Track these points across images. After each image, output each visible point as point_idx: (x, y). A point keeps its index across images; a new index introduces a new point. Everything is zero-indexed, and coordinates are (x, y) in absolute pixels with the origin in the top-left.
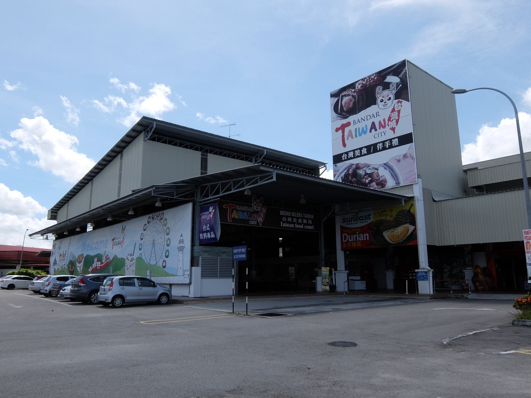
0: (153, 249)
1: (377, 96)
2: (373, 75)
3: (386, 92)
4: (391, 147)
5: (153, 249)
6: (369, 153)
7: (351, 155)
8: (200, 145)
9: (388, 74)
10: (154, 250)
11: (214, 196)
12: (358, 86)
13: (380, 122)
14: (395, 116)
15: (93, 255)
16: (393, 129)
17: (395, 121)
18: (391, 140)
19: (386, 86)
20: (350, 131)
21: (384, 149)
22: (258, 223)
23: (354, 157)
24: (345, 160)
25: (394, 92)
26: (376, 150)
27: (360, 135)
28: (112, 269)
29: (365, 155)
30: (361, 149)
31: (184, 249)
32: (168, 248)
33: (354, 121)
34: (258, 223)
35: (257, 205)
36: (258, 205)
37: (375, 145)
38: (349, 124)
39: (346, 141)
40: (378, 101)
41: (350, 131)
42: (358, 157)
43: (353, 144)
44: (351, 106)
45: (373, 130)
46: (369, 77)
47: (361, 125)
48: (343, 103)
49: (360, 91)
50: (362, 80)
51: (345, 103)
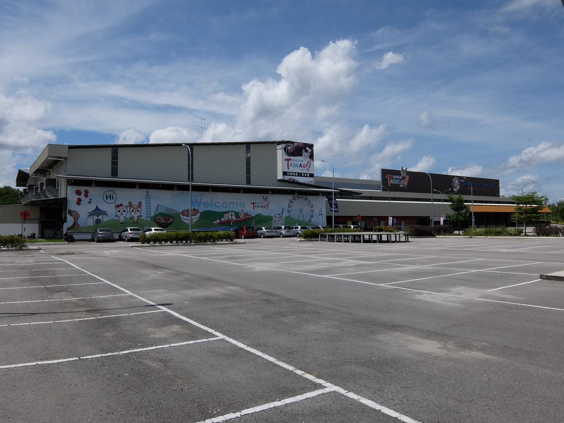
0: (301, 214)
1: (303, 153)
2: (302, 143)
3: (306, 153)
4: (307, 176)
5: (301, 214)
6: (298, 176)
7: (294, 174)
8: (130, 228)
9: (307, 146)
10: (301, 214)
11: (74, 267)
12: (295, 145)
13: (303, 165)
14: (309, 164)
15: (265, 215)
16: (308, 170)
17: (308, 167)
18: (307, 174)
19: (306, 151)
20: (291, 163)
21: (304, 176)
22: (404, 186)
23: (292, 176)
24: (288, 175)
25: (309, 155)
26: (301, 176)
27: (295, 167)
28: (522, 177)
29: (297, 176)
30: (295, 173)
31: (79, 223)
32: (312, 213)
33: (293, 160)
34: (404, 186)
35: (135, 211)
36: (137, 210)
37: (301, 173)
38: (290, 160)
39: (289, 167)
40: (303, 155)
41: (291, 163)
42: (294, 176)
43: (292, 169)
44: (292, 152)
45: (301, 167)
46: (300, 143)
47: (296, 163)
48: (288, 148)
49: (296, 147)
50: (297, 142)
51: (289, 149)
